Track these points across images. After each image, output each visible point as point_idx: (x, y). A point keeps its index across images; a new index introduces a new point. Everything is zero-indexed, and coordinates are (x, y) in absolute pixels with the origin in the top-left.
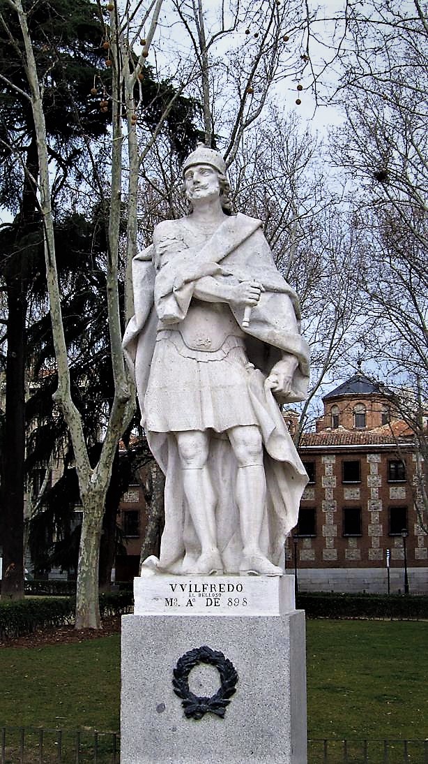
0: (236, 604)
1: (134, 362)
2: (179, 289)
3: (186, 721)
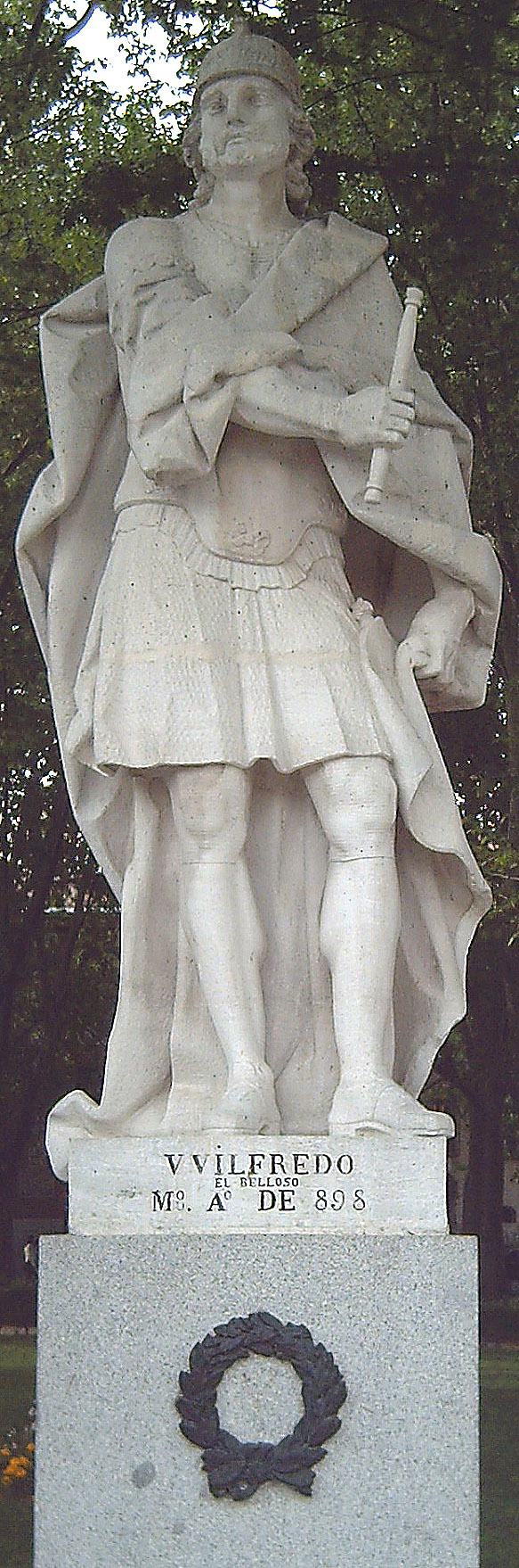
1: (45, 588)
2: (202, 396)
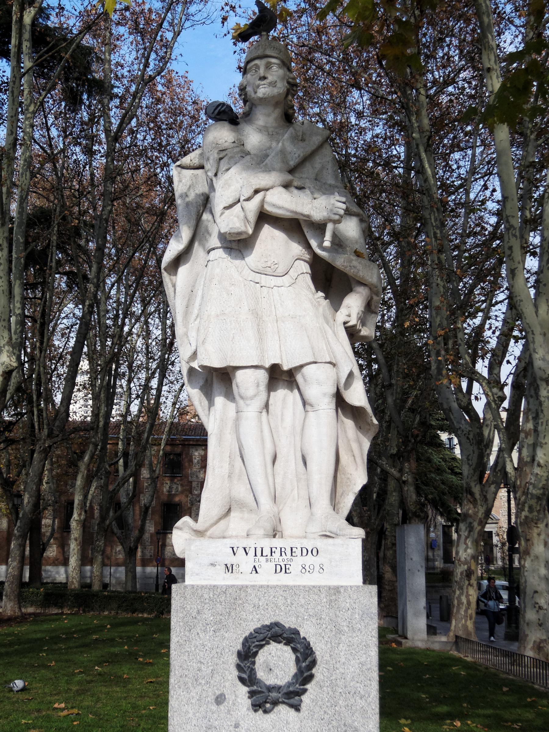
0: (311, 571)
2: (248, 199)
3: (251, 714)
